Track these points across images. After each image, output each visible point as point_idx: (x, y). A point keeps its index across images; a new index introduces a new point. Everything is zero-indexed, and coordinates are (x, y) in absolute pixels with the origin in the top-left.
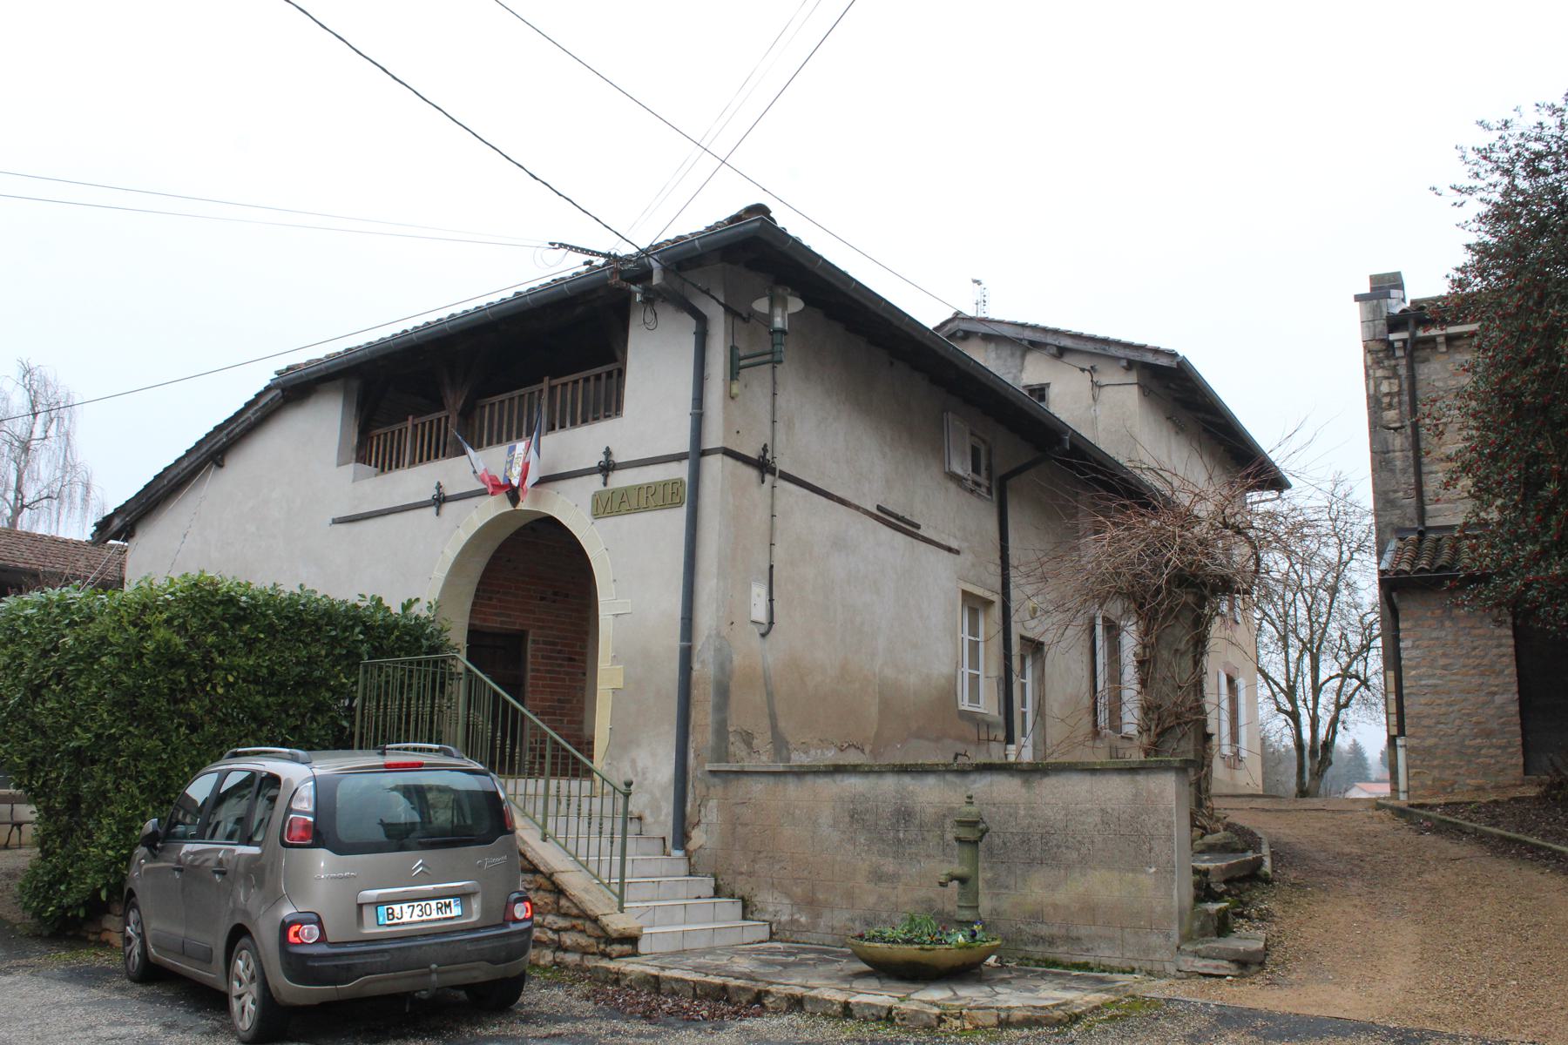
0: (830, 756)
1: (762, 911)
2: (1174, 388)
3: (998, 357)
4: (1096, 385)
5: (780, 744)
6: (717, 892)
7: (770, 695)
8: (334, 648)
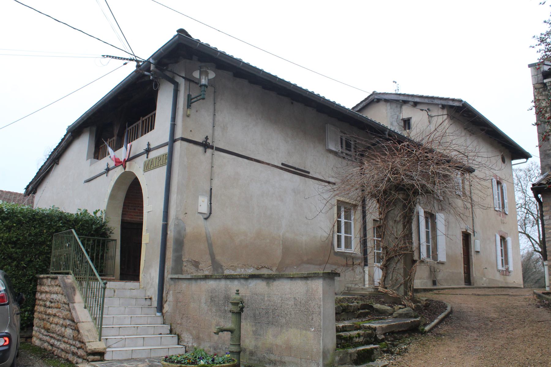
0: (251, 271)
1: (184, 341)
2: (464, 116)
3: (391, 108)
4: (430, 117)
5: (216, 265)
6: (171, 332)
7: (210, 246)
8: (50, 229)
